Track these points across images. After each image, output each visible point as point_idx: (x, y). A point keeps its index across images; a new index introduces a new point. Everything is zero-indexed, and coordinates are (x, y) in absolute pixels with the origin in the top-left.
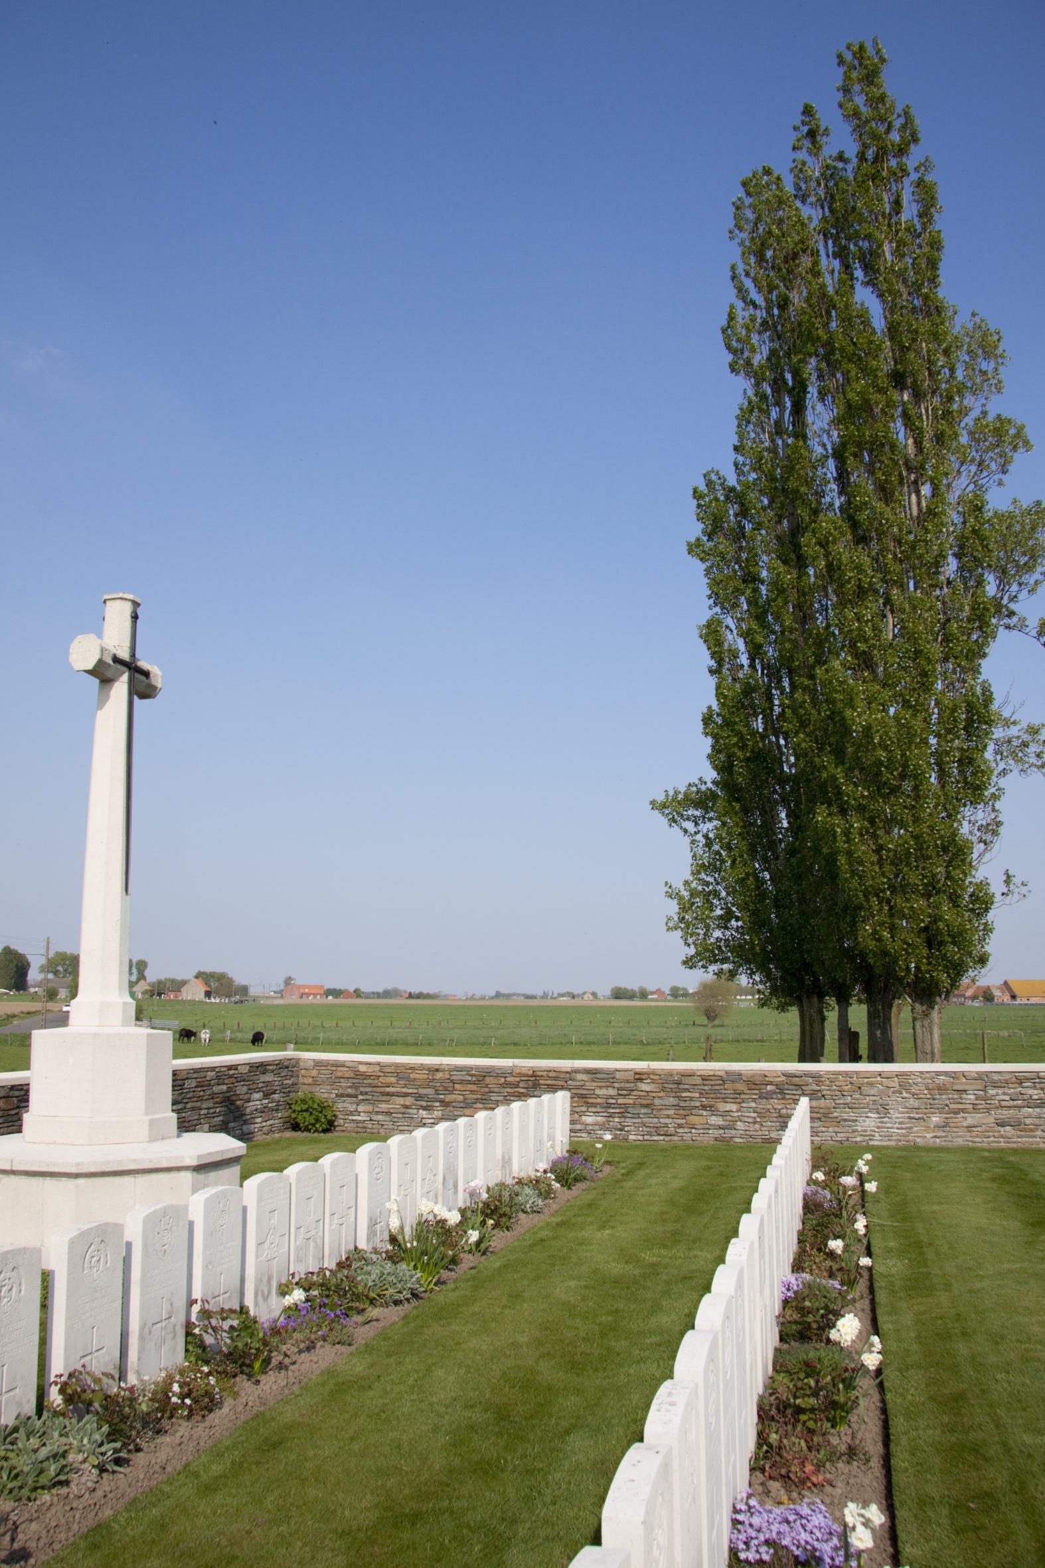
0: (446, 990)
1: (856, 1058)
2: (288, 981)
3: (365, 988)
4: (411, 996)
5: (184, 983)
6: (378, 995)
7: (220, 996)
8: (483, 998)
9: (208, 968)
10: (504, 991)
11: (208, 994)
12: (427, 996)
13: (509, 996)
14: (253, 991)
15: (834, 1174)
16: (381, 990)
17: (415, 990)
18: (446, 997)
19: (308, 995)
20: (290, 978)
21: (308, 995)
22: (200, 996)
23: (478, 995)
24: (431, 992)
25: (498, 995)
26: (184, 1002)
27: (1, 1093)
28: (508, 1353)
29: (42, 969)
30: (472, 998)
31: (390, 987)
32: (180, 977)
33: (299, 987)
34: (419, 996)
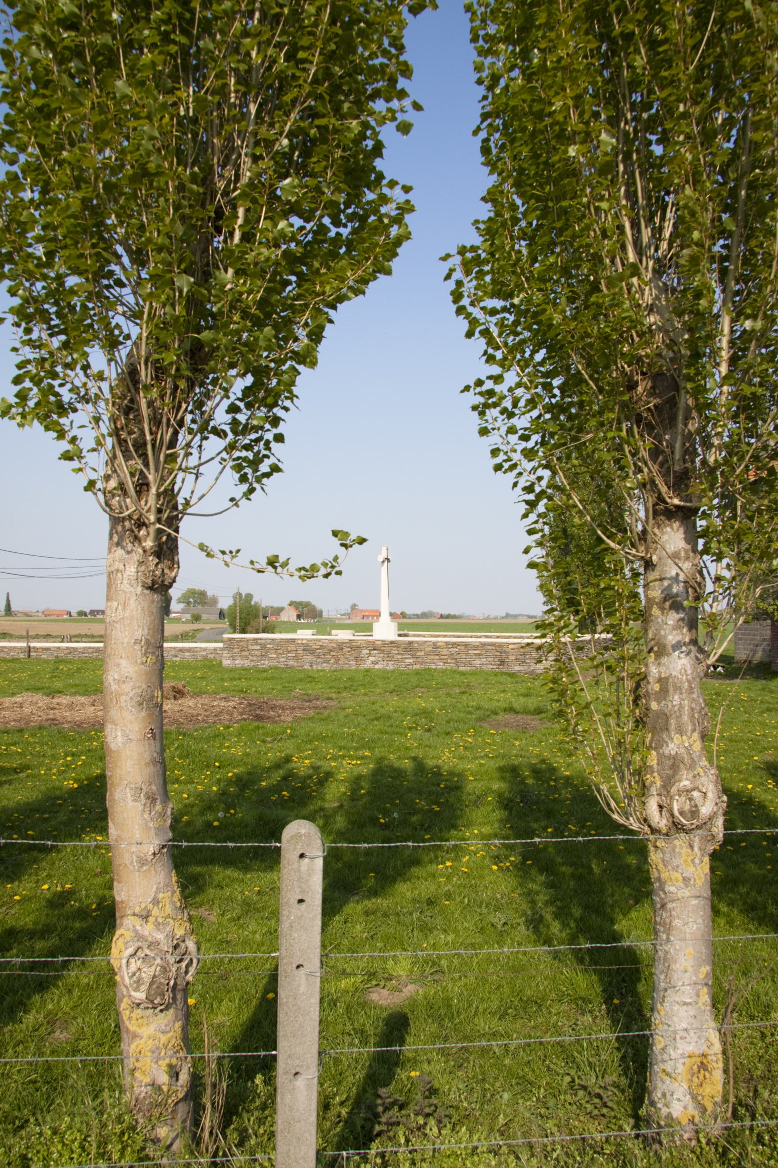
0: (468, 612)
1: (234, 632)
2: (354, 607)
3: (409, 612)
4: (442, 617)
5: (282, 609)
6: (417, 616)
7: (308, 618)
8: (496, 618)
9: (298, 599)
10: (512, 612)
11: (299, 617)
12: (454, 617)
13: (515, 616)
14: (325, 615)
15: (115, 423)
16: (419, 612)
17: (445, 612)
18: (468, 617)
19: (368, 616)
20: (355, 605)
21: (368, 616)
22: (293, 618)
23: (493, 616)
24: (457, 613)
25: (508, 616)
26: (284, 623)
27: (1, 727)
28: (69, 359)
29: (179, 601)
30: (488, 618)
31: (426, 610)
32: (276, 605)
33: (362, 611)
34: (448, 617)
